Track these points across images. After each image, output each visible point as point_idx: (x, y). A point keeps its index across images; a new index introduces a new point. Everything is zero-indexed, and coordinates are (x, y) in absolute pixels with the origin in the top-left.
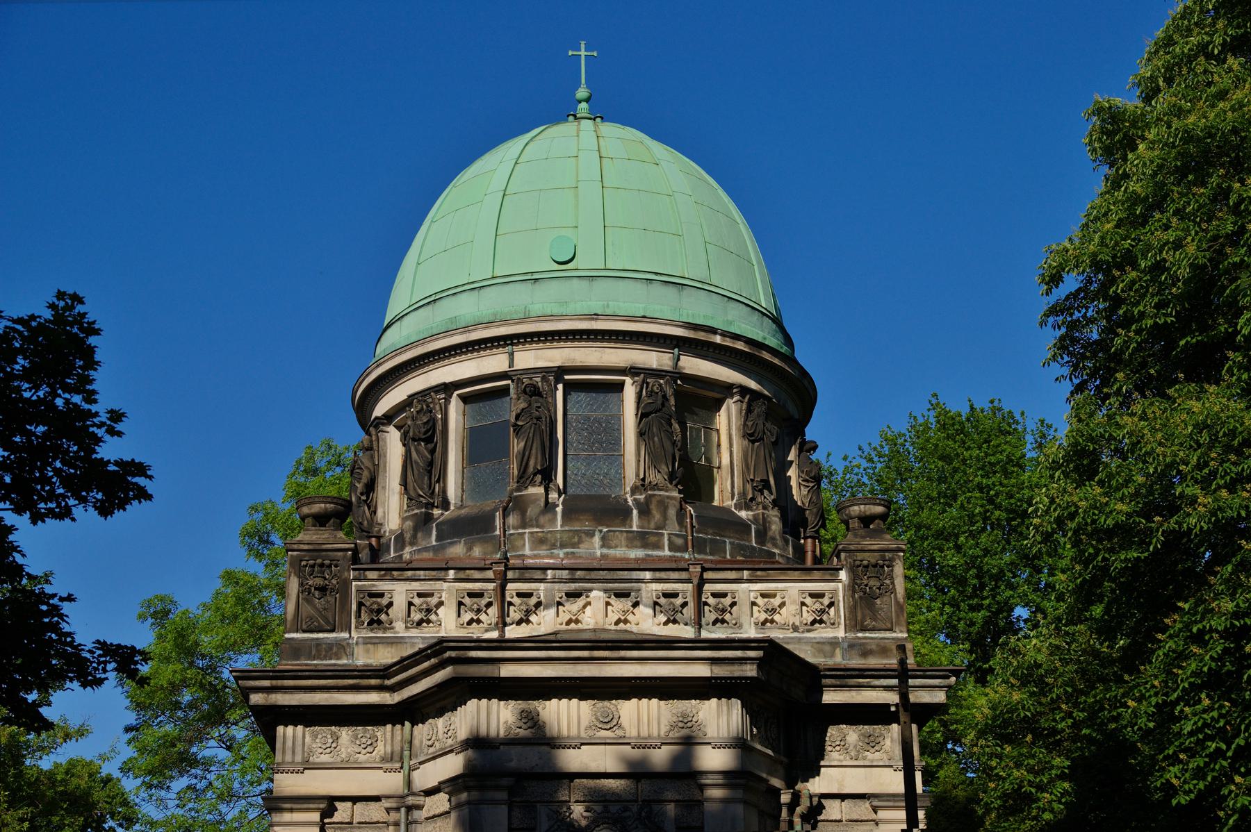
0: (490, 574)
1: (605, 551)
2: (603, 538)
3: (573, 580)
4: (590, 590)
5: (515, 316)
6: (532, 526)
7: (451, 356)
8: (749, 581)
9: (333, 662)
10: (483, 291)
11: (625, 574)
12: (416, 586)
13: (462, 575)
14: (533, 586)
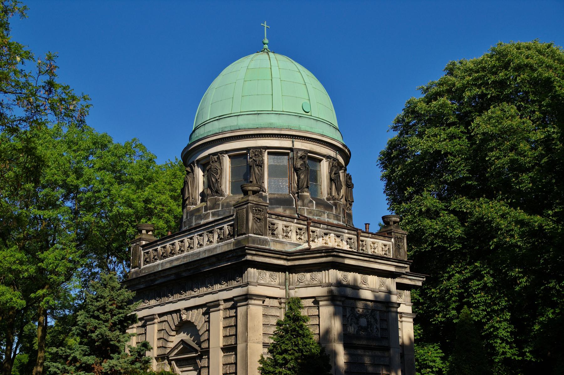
0: (306, 223)
1: (328, 220)
2: (328, 215)
3: (327, 229)
4: (331, 233)
5: (296, 129)
6: (306, 206)
7: (309, 140)
8: (371, 238)
9: (264, 247)
10: (280, 115)
11: (340, 230)
12: (285, 223)
13: (298, 221)
14: (316, 229)
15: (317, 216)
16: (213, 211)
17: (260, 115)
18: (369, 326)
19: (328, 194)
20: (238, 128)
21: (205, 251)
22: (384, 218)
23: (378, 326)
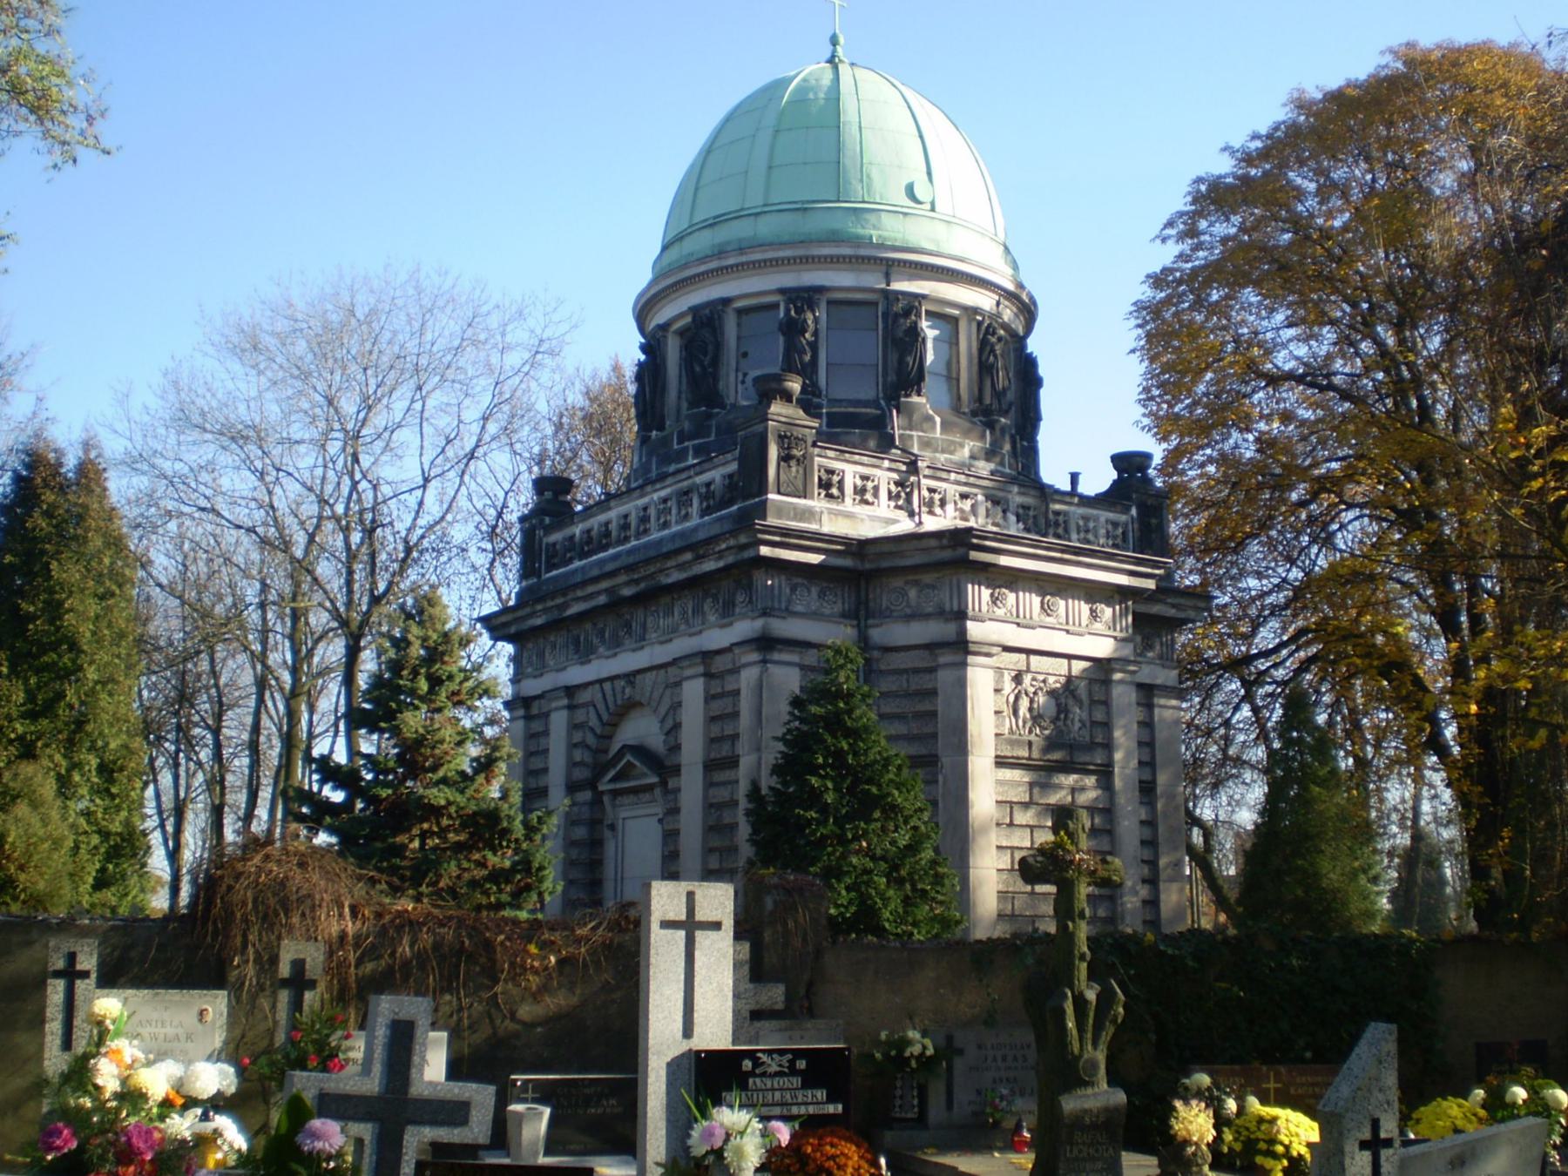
3: (966, 484)
6: (917, 430)
15: (943, 451)
16: (696, 442)
18: (1062, 716)
21: (673, 537)
22: (1120, 461)
23: (1085, 715)
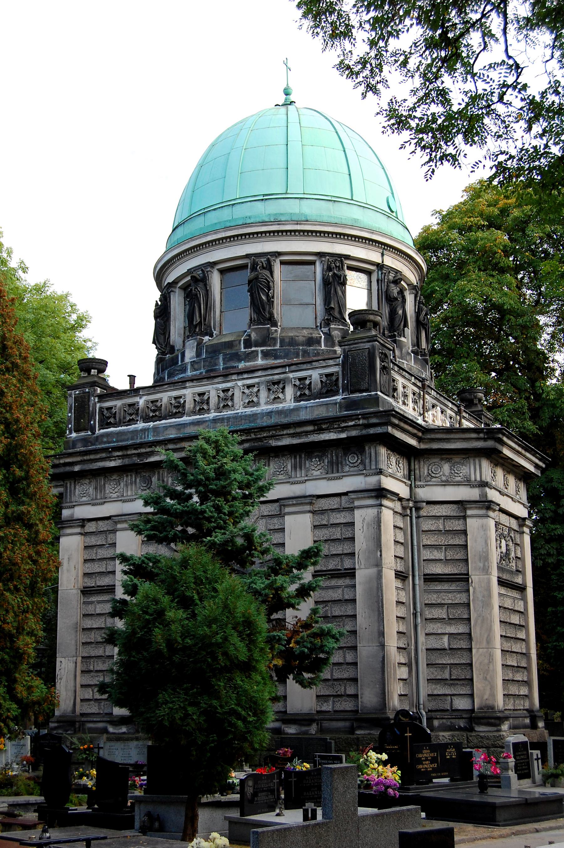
17: (336, 203)
19: (413, 346)
20: (303, 219)
